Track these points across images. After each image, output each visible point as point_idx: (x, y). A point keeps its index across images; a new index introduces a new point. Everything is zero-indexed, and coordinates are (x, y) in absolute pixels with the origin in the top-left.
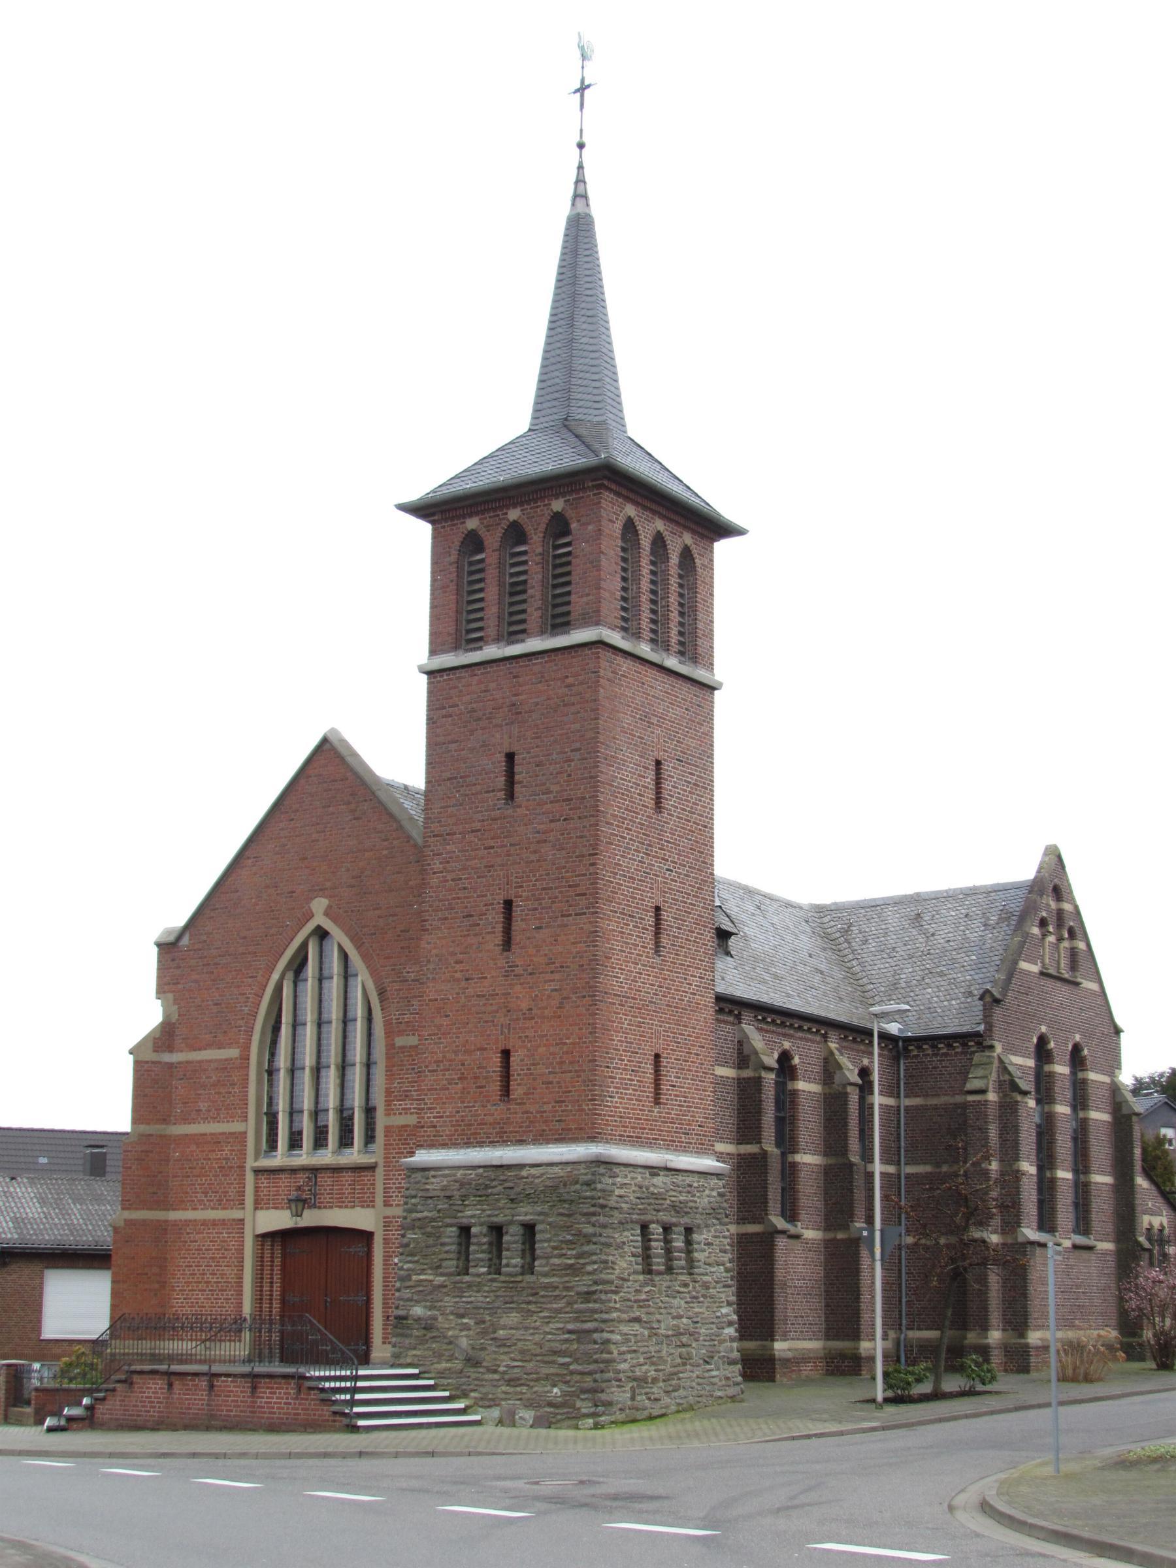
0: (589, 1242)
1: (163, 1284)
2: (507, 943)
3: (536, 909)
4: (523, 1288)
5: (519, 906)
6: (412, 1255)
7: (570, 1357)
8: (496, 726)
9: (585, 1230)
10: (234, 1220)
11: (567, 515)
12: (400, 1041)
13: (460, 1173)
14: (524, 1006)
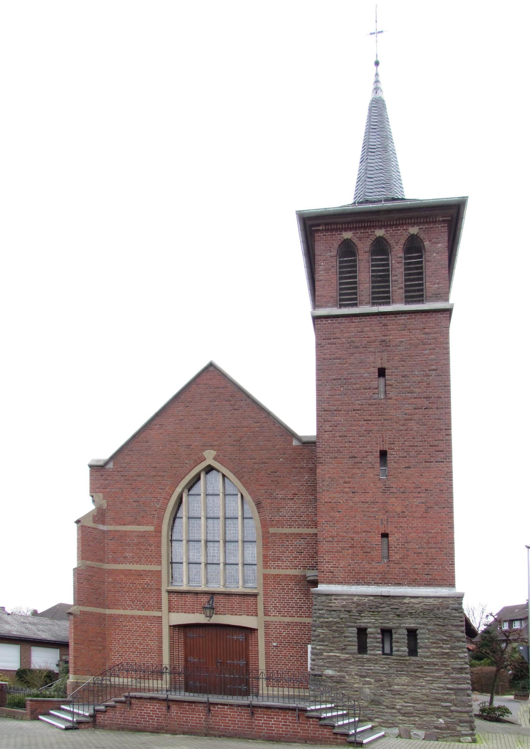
0: (459, 641)
1: (104, 647)
3: (406, 457)
4: (411, 664)
5: (392, 454)
6: (322, 641)
7: (451, 703)
8: (371, 352)
9: (456, 635)
10: (154, 617)
11: (421, 237)
12: (272, 530)
13: (355, 599)
14: (398, 510)
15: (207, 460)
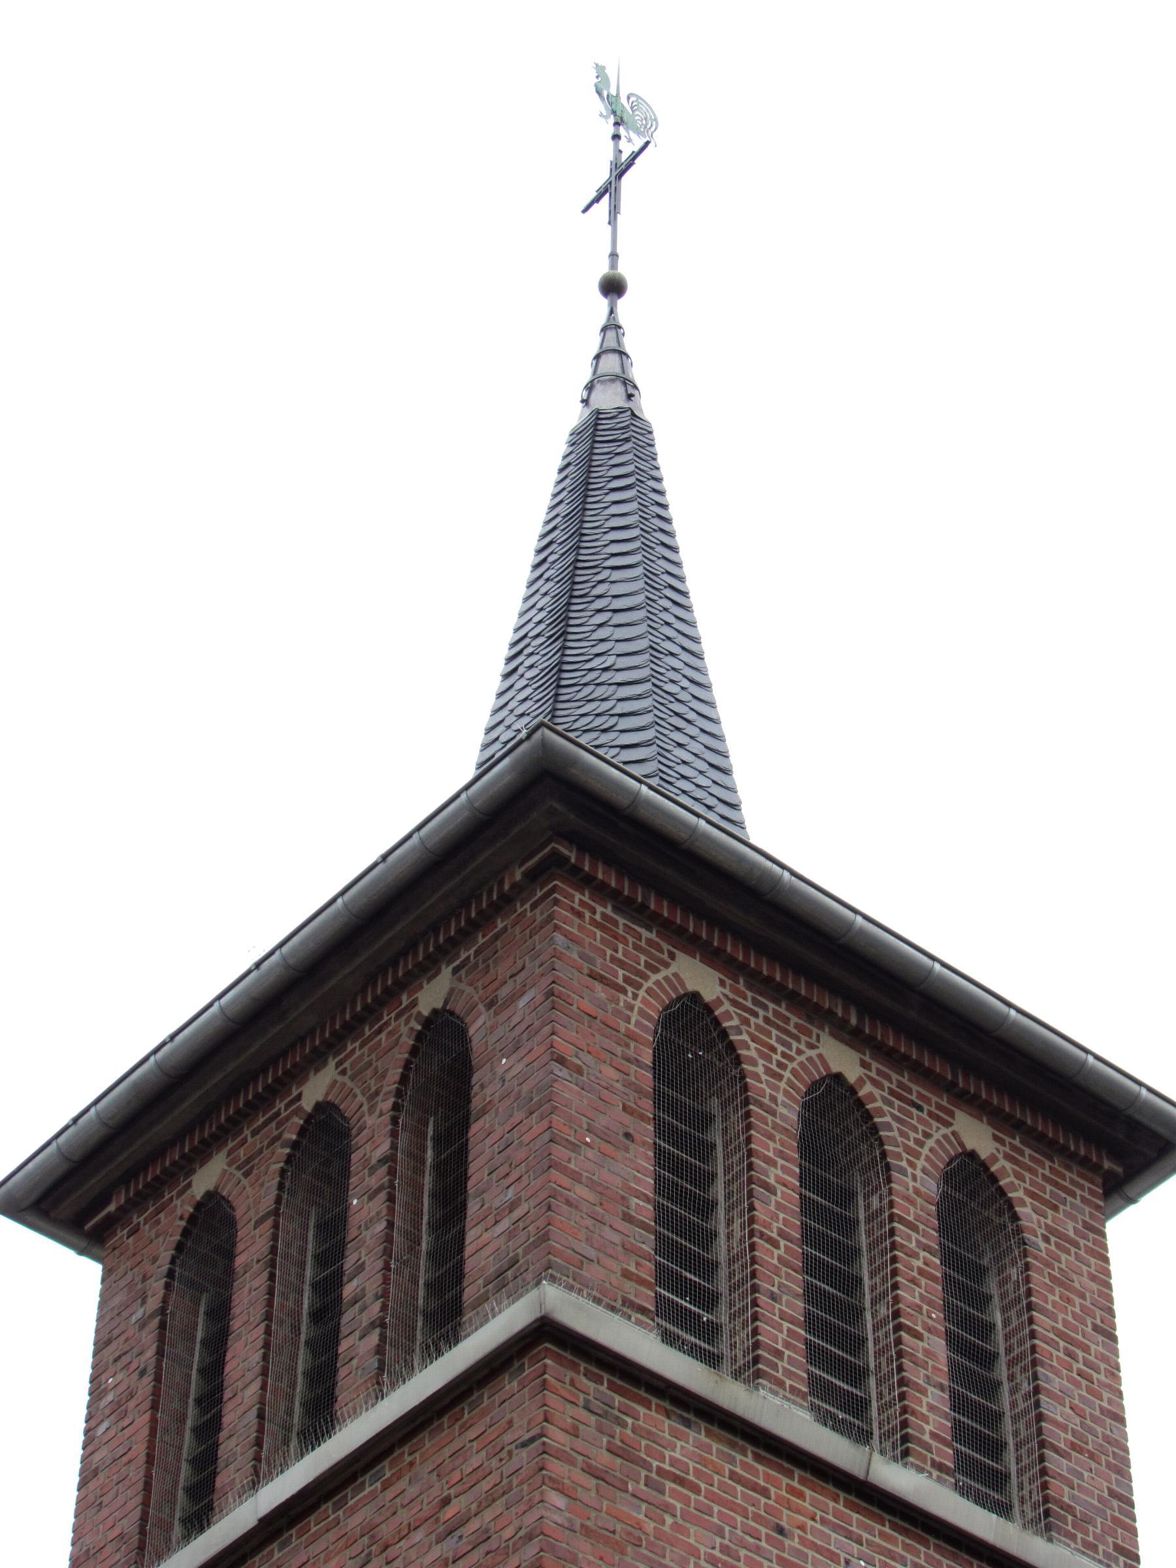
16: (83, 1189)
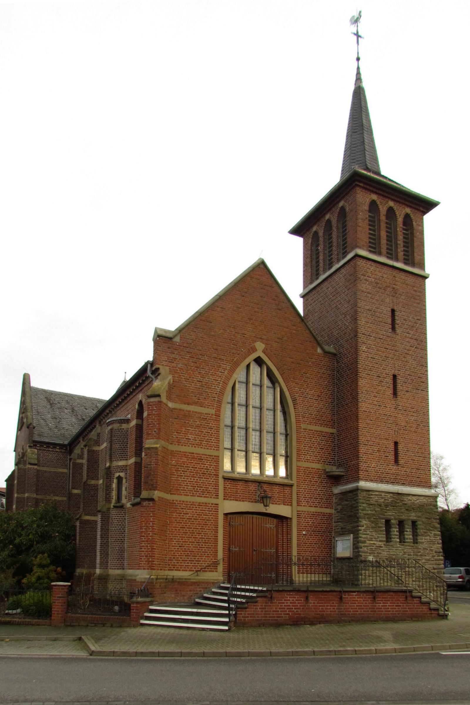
2: (395, 394)
10: (212, 504)
14: (403, 424)
15: (258, 351)
16: (298, 230)
